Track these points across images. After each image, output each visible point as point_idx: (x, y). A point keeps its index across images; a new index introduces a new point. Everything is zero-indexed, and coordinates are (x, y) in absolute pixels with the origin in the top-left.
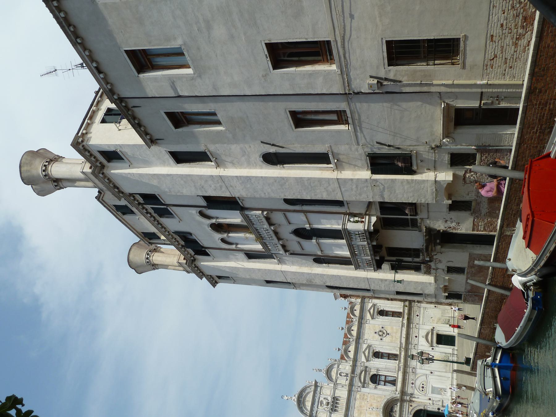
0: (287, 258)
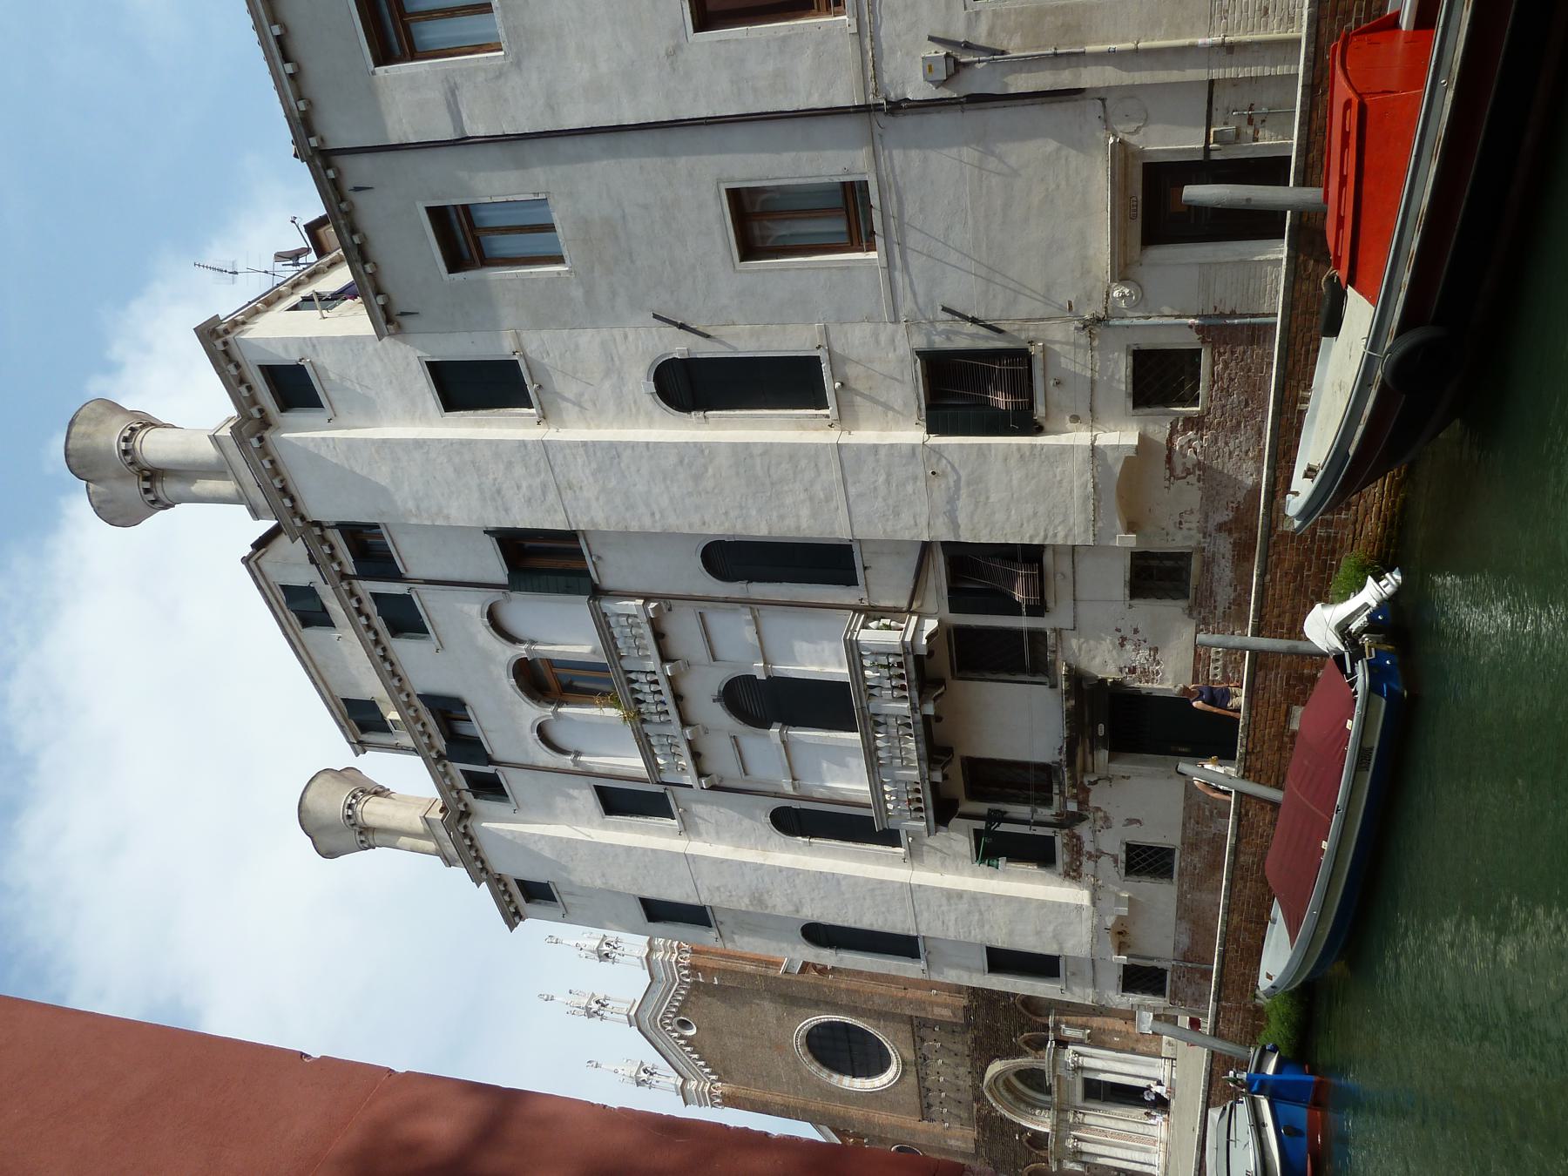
0: (708, 810)
